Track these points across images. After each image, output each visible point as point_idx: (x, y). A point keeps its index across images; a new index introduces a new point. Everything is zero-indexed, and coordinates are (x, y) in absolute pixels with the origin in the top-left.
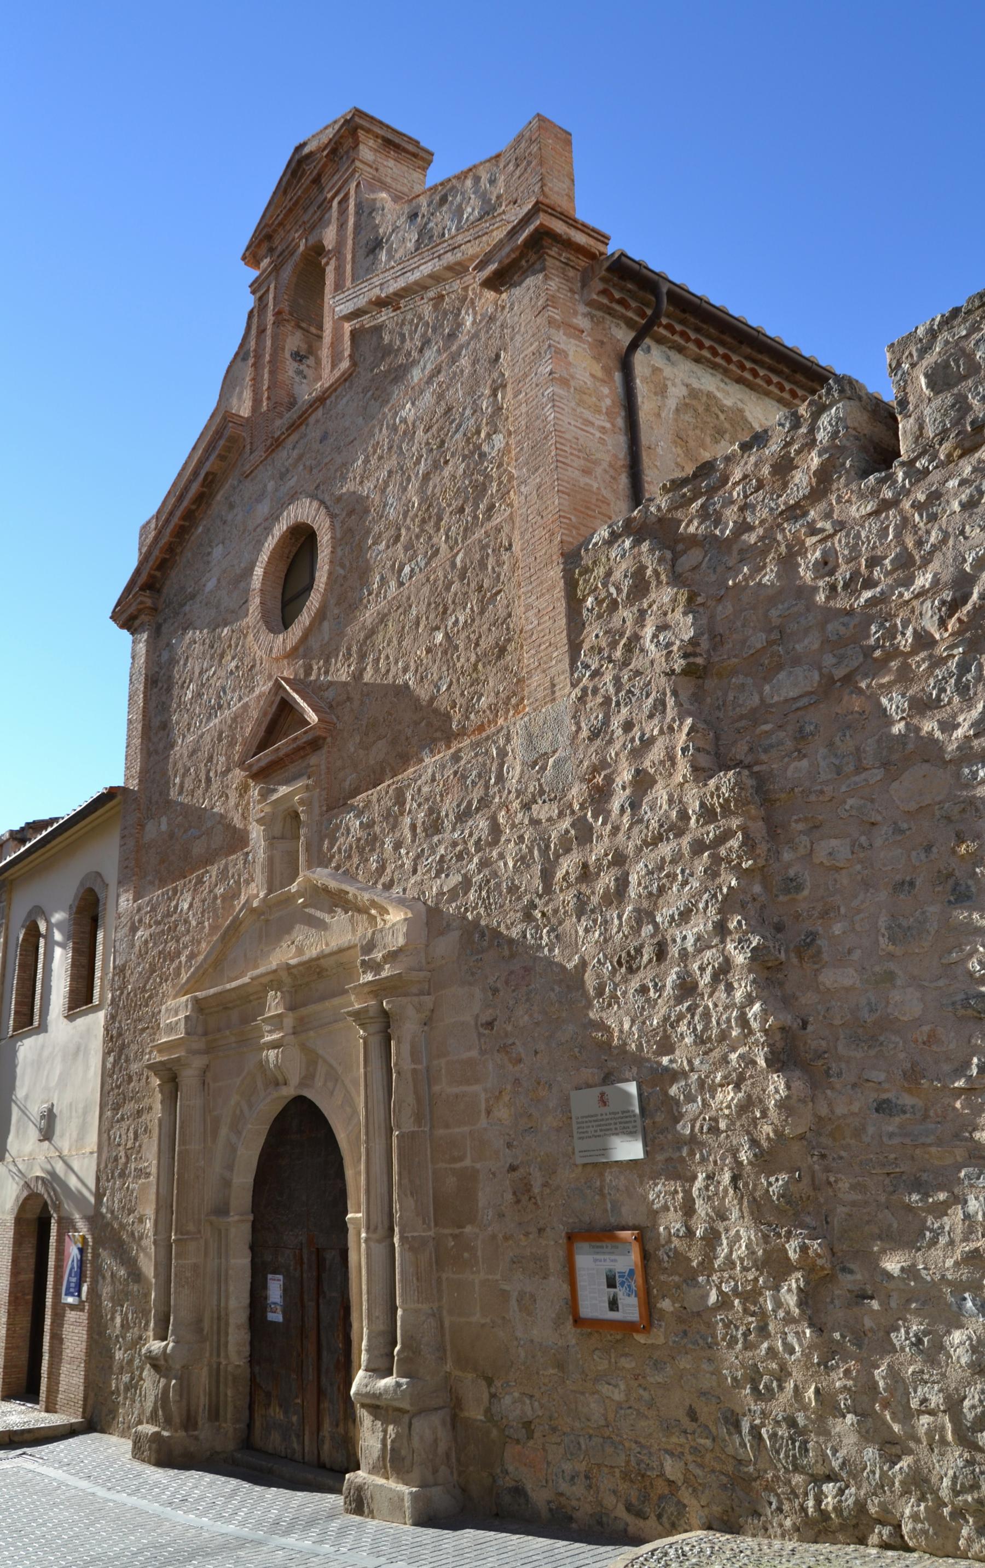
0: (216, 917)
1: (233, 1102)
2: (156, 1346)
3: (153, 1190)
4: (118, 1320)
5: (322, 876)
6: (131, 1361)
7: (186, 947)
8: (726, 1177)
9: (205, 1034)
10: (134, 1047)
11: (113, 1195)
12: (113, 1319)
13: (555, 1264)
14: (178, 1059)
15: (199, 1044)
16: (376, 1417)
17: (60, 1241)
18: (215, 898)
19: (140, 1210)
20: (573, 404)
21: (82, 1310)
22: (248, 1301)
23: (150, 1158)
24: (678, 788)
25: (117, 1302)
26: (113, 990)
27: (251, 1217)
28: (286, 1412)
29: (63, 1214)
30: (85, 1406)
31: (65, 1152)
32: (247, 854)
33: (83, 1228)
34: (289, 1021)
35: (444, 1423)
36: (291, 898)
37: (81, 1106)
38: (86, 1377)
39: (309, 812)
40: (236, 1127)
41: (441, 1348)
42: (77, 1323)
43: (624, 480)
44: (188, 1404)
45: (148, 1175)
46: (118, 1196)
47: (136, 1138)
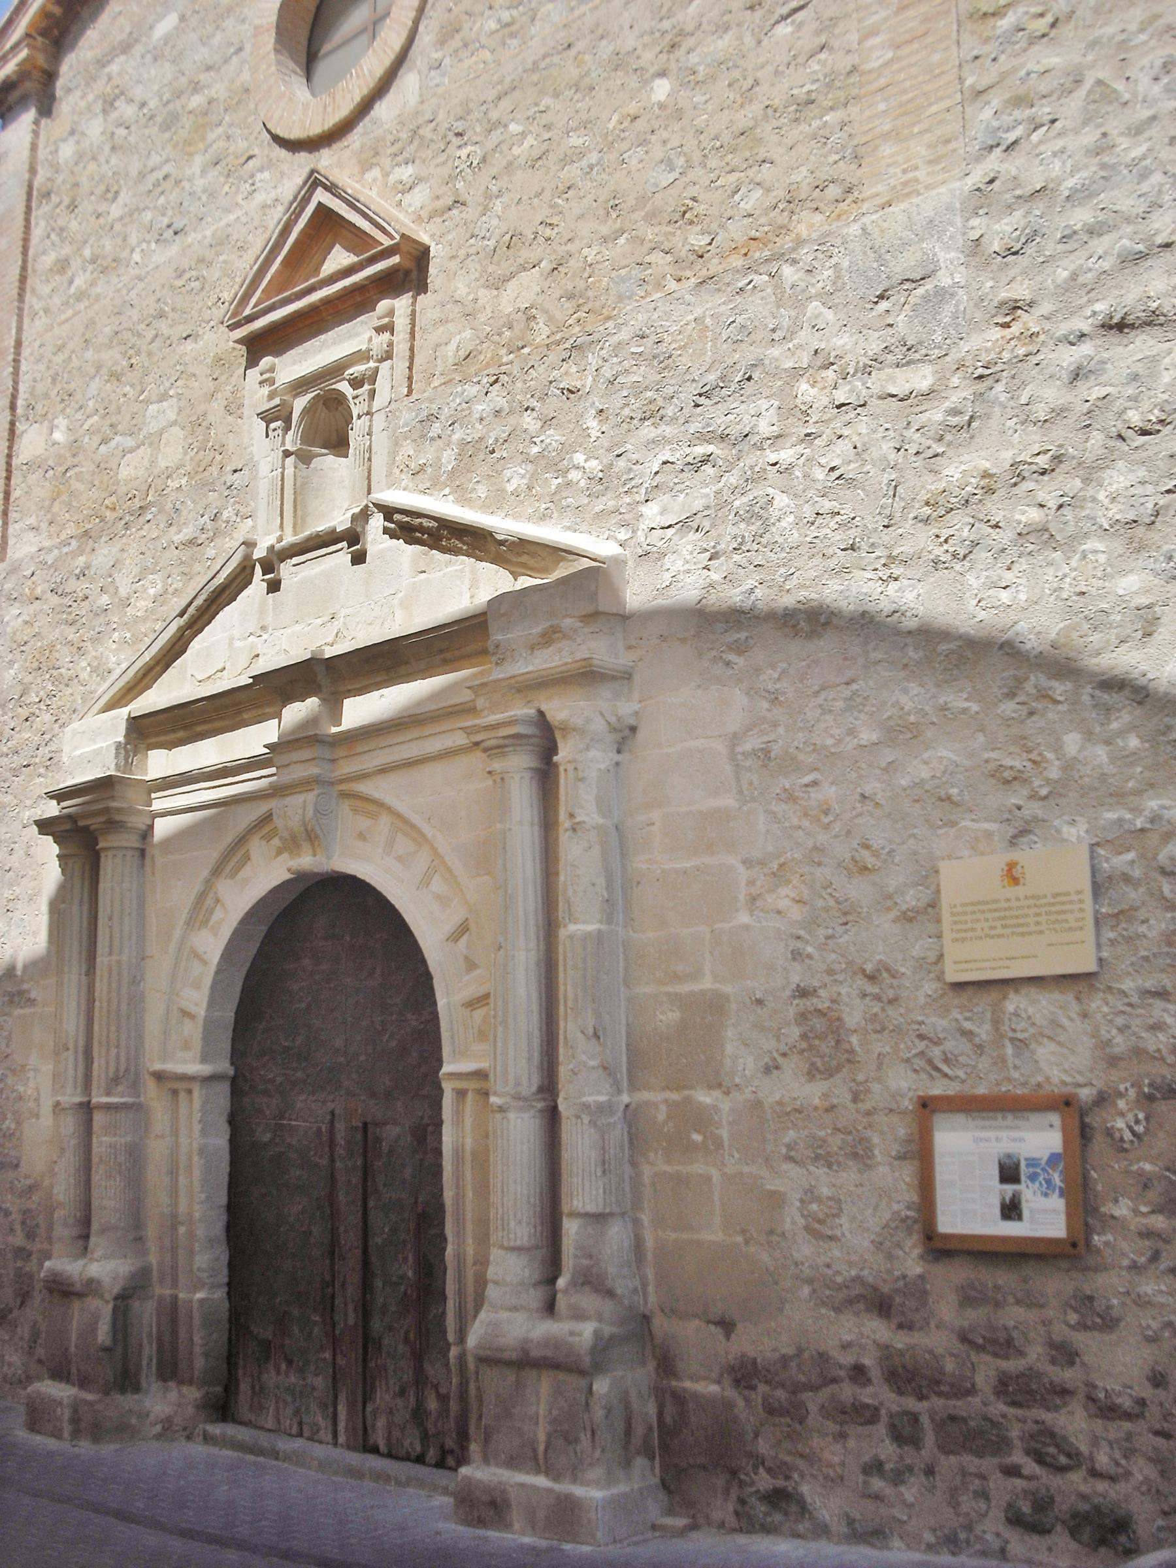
22: (224, 1200)
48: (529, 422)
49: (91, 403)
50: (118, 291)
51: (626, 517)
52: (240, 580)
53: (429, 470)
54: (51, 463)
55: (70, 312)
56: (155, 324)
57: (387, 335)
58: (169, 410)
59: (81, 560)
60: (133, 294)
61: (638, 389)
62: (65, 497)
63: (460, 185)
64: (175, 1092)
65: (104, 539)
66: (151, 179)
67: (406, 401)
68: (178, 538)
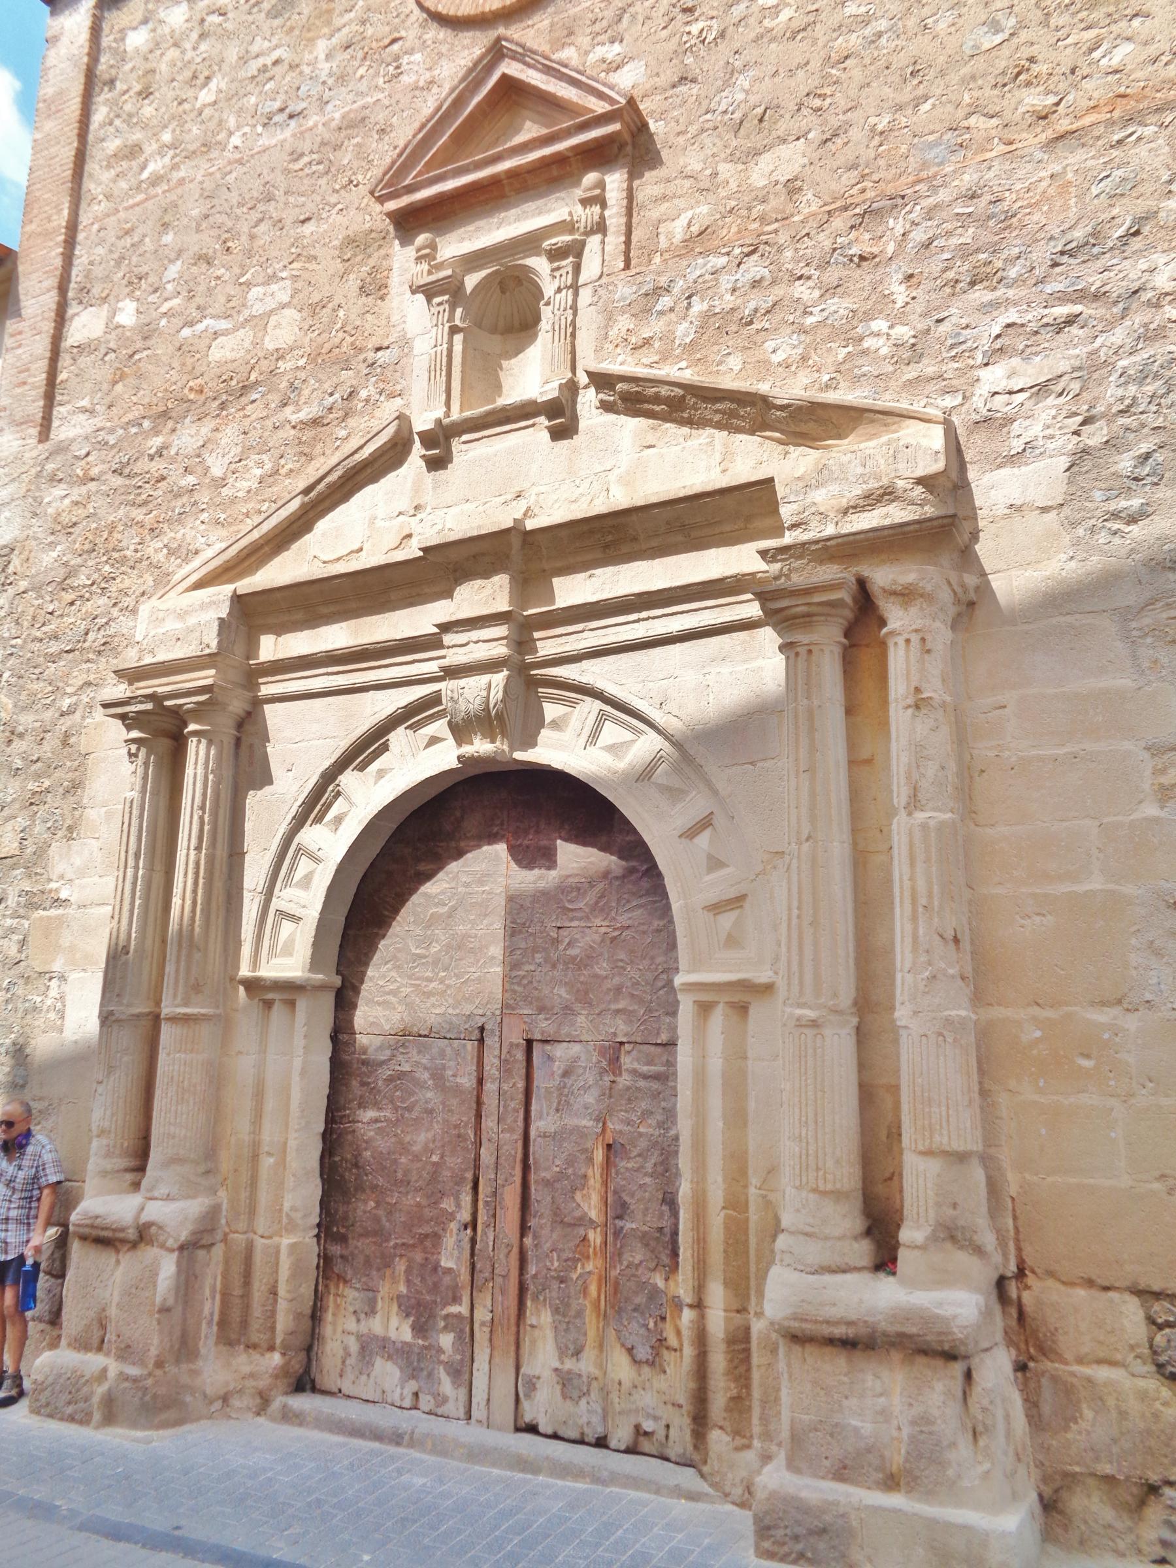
48: (801, 290)
49: (169, 287)
50: (211, 174)
51: (954, 382)
52: (392, 455)
53: (657, 344)
54: (112, 345)
55: (140, 197)
56: (261, 207)
57: (596, 209)
58: (281, 292)
59: (158, 441)
60: (230, 178)
61: (965, 252)
62: (131, 381)
63: (689, 60)
64: (268, 1004)
65: (187, 420)
66: (254, 66)
67: (623, 275)
68: (294, 418)
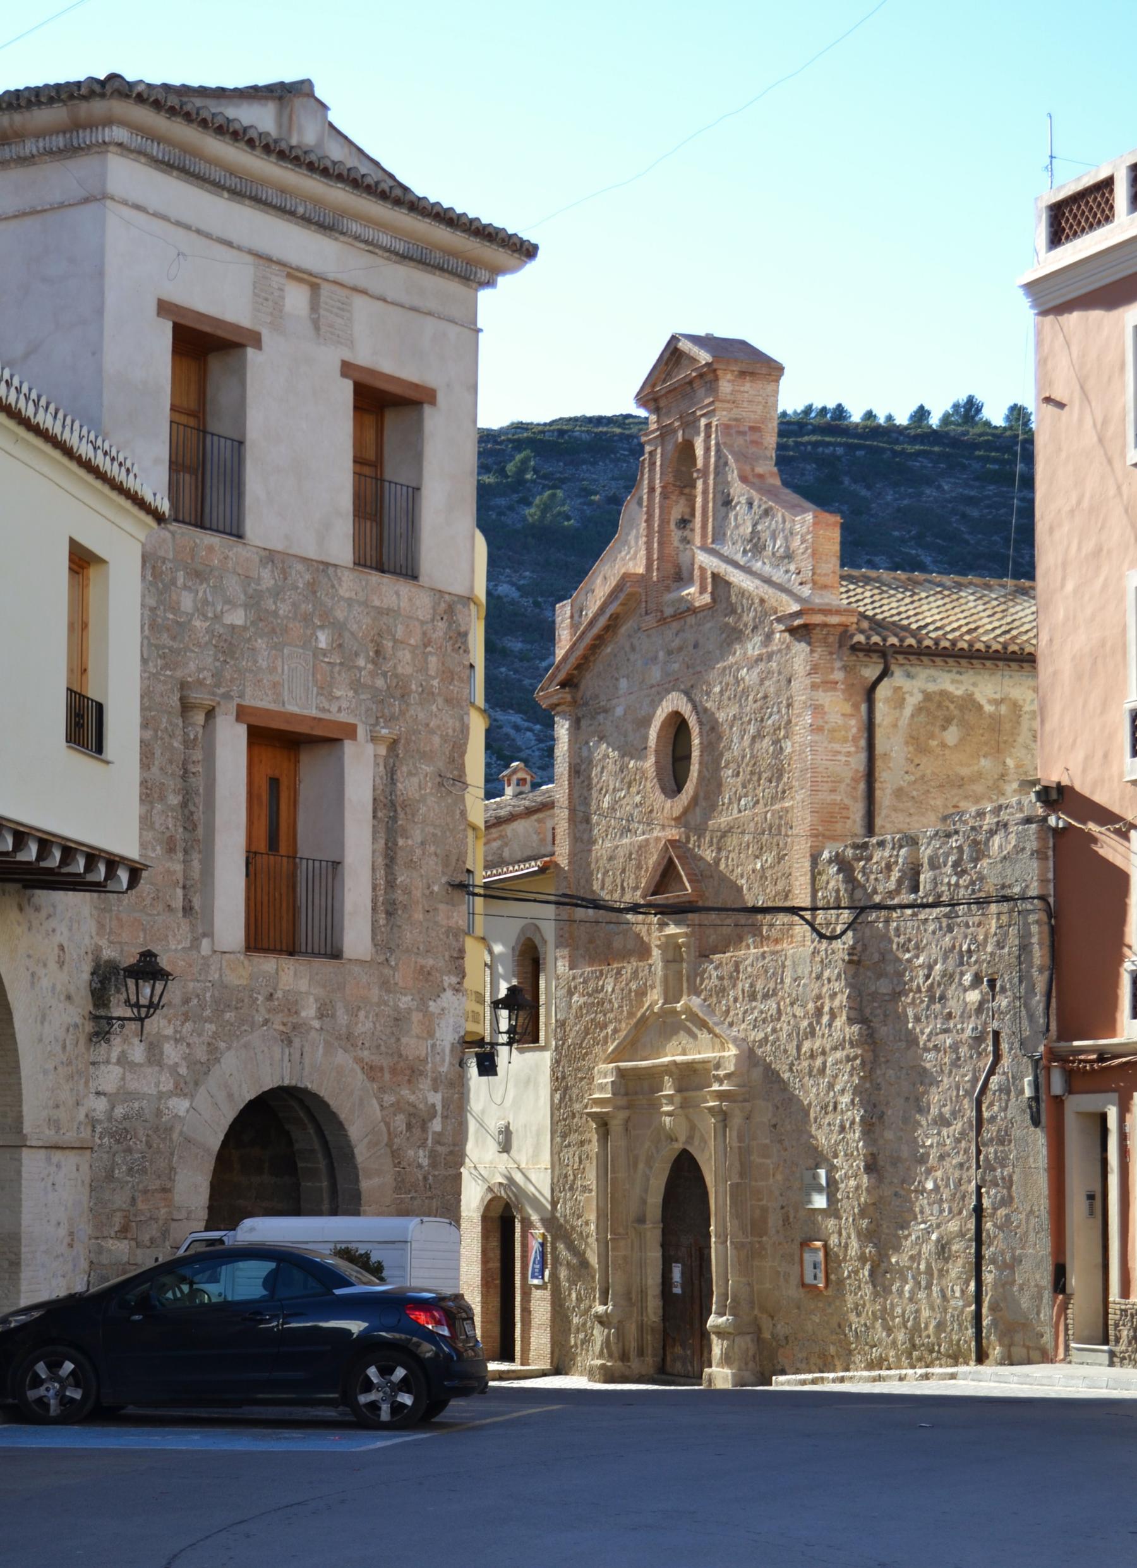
0: (631, 1006)
1: (646, 1147)
2: (600, 1309)
3: (595, 1203)
4: (574, 1295)
5: (695, 1002)
6: (584, 1324)
7: (611, 1022)
8: (851, 1220)
9: (627, 1094)
10: (575, 1091)
11: (565, 1203)
12: (570, 1295)
13: (797, 1259)
14: (607, 1113)
15: (622, 1101)
16: (719, 1338)
17: (524, 1236)
18: (630, 991)
19: (586, 1216)
20: (825, 744)
21: (546, 1289)
23: (591, 1178)
24: (843, 1028)
25: (573, 1282)
26: (557, 1040)
27: (661, 1225)
28: (684, 1349)
29: (525, 1215)
30: (552, 1358)
31: (523, 1166)
32: (651, 966)
33: (539, 1231)
34: (678, 1099)
35: (752, 1340)
36: (674, 1012)
37: (534, 1128)
38: (552, 1338)
39: (688, 953)
40: (649, 1163)
41: (752, 1302)
42: (542, 1299)
43: (862, 786)
44: (623, 1346)
45: (591, 1191)
46: (569, 1205)
47: (580, 1162)
